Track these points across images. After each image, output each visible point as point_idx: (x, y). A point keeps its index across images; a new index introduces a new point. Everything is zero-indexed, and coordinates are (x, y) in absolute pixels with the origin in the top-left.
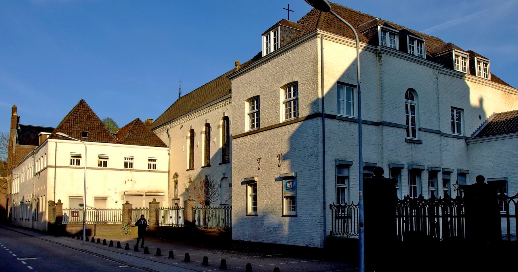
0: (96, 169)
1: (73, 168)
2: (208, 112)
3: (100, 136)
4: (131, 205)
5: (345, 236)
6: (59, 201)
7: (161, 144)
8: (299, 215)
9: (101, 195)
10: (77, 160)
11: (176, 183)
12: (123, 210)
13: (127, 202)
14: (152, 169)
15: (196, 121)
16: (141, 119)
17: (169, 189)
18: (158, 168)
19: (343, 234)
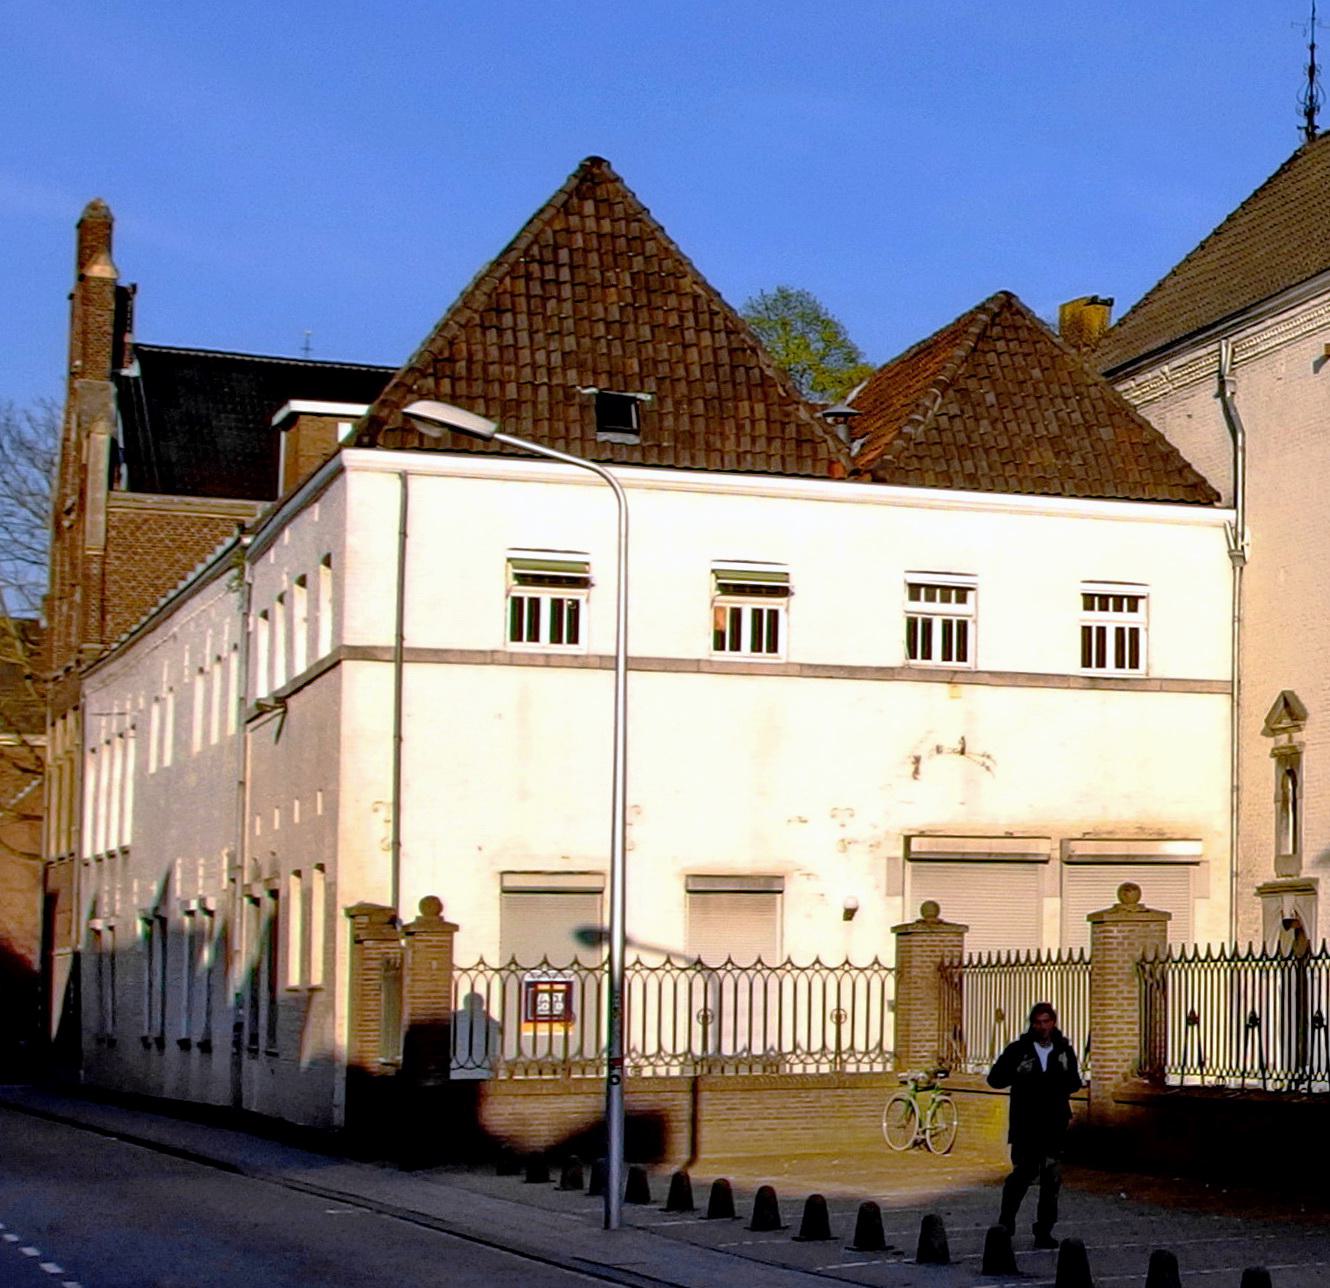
0: (696, 666)
1: (530, 661)
3: (730, 428)
4: (960, 930)
6: (432, 905)
10: (557, 604)
12: (901, 972)
13: (931, 910)
14: (1110, 670)
17: (1235, 810)
18: (1156, 658)
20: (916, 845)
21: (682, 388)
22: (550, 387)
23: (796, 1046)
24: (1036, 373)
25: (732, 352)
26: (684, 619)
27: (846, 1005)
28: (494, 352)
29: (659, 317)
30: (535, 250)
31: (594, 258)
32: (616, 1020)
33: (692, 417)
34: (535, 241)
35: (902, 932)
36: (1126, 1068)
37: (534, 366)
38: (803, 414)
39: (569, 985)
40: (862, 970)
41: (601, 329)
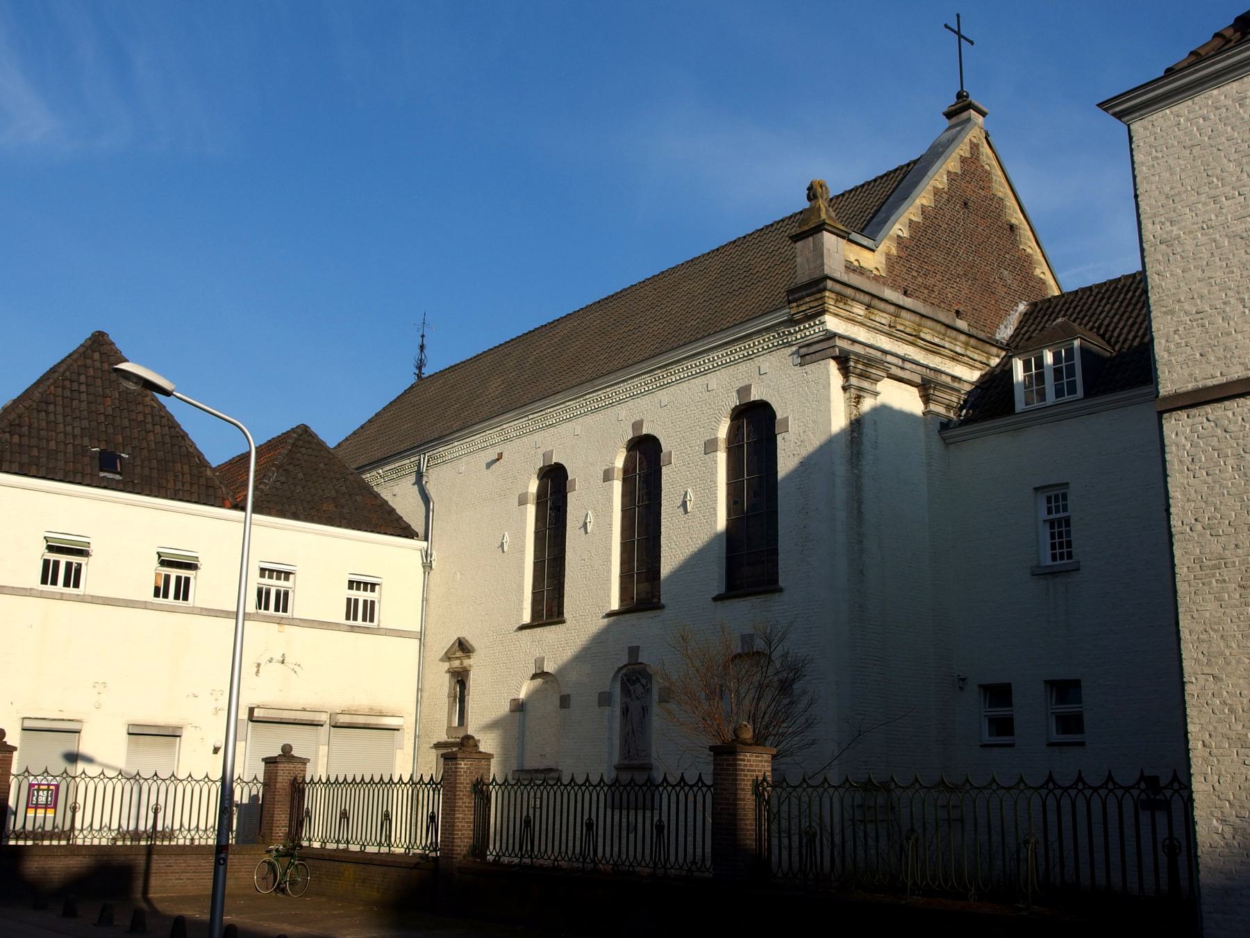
0: (144, 605)
1: (51, 596)
2: (649, 392)
3: (170, 477)
4: (304, 762)
7: (387, 522)
10: (69, 565)
11: (460, 679)
13: (287, 749)
14: (360, 622)
15: (587, 438)
16: (314, 428)
17: (418, 702)
18: (384, 616)
19: (585, 859)
20: (257, 713)
21: (145, 453)
22: (74, 446)
23: (181, 825)
24: (322, 465)
25: (171, 437)
27: (162, 802)
28: (44, 424)
29: (134, 417)
30: (68, 373)
31: (99, 382)
32: (225, 822)
33: (151, 469)
34: (68, 369)
35: (269, 761)
36: (464, 852)
37: (66, 434)
38: (209, 473)
39: (57, 787)
40: (92, 778)
41: (102, 418)
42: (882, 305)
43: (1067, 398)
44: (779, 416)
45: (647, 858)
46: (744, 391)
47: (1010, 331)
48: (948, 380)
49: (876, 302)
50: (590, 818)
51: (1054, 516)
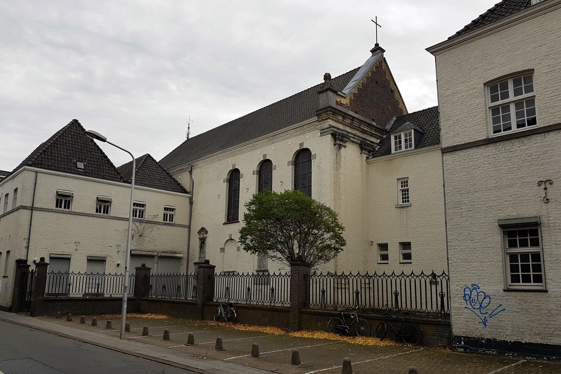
0: (93, 216)
4: (149, 269)
5: (273, 304)
8: (550, 288)
9: (97, 253)
13: (143, 265)
14: (168, 221)
15: (247, 160)
18: (176, 220)
26: (91, 207)
27: (398, 290)
42: (348, 117)
43: (409, 149)
44: (274, 164)
45: (318, 302)
46: (301, 144)
47: (390, 127)
48: (369, 142)
49: (345, 116)
50: (323, 289)
51: (403, 188)
